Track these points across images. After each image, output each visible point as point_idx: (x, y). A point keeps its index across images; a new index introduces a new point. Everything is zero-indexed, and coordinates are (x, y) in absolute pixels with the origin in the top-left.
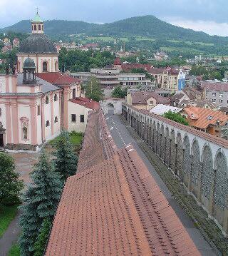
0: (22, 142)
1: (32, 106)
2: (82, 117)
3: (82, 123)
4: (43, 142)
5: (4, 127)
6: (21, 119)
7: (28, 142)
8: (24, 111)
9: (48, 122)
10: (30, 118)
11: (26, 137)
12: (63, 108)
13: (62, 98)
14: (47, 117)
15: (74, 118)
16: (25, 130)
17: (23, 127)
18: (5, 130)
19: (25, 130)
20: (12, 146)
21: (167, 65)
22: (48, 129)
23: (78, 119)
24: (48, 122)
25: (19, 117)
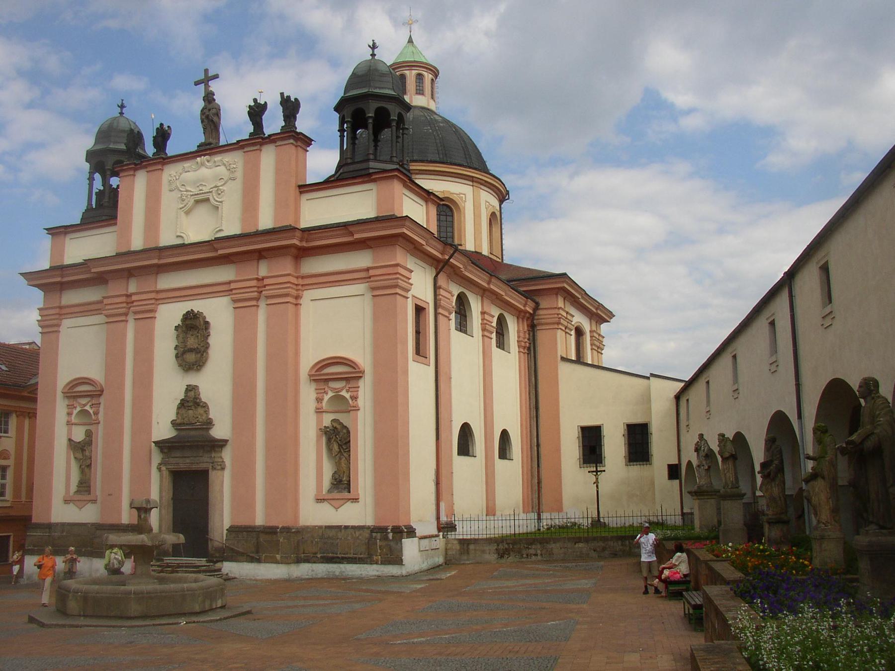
0: (314, 513)
2: (638, 440)
3: (636, 470)
4: (446, 528)
5: (220, 431)
6: (73, 391)
7: (357, 513)
8: (334, 320)
9: (466, 431)
11: (342, 483)
13: (530, 350)
16: (338, 440)
17: (327, 420)
18: (220, 444)
19: (338, 440)
20: (257, 542)
22: (466, 472)
23: (614, 446)
24: (466, 431)
25: (309, 358)
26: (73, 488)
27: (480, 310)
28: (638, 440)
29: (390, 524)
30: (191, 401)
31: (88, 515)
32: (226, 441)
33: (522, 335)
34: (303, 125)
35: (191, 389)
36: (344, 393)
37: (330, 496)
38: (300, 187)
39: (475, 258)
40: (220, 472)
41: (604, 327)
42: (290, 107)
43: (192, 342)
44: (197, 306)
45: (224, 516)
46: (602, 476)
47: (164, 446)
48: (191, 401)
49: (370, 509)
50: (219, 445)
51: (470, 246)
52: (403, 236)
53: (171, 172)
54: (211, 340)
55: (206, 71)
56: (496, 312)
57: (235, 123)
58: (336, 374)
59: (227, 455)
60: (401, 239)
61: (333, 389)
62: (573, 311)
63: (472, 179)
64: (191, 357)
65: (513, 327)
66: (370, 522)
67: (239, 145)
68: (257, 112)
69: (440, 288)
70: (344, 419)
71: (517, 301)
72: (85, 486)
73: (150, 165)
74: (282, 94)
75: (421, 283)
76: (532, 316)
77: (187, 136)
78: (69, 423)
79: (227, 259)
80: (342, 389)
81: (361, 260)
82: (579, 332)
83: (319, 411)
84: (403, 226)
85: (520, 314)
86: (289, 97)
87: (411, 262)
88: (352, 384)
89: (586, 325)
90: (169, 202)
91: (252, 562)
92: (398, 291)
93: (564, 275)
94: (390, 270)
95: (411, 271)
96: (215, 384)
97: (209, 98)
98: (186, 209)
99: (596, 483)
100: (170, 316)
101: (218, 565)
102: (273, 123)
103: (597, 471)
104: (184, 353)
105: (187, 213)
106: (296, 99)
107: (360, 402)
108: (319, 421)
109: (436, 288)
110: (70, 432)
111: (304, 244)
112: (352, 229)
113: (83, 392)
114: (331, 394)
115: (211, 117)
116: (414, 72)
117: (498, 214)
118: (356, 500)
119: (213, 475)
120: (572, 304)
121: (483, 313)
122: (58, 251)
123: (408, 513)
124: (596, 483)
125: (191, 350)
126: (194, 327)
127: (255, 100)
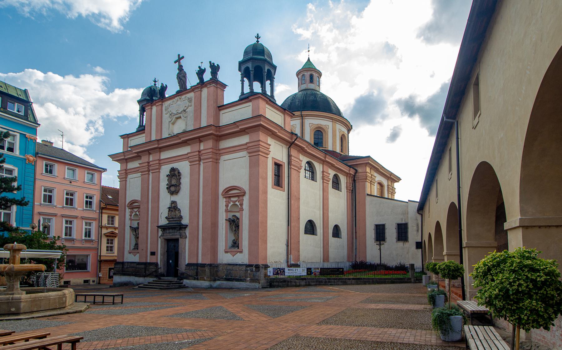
0: (225, 258)
2: (402, 232)
3: (401, 244)
5: (185, 221)
6: (229, 192)
7: (242, 258)
9: (336, 228)
10: (246, 188)
11: (236, 245)
16: (234, 224)
17: (230, 215)
18: (186, 226)
19: (234, 224)
23: (391, 233)
25: (222, 186)
26: (132, 247)
27: (321, 170)
28: (402, 232)
29: (254, 263)
30: (173, 207)
31: (136, 258)
32: (187, 226)
33: (348, 184)
34: (221, 77)
35: (173, 202)
36: (237, 203)
37: (230, 250)
38: (219, 107)
39: (333, 154)
40: (184, 240)
41: (396, 185)
42: (215, 69)
43: (174, 182)
44: (175, 165)
45: (186, 258)
46: (382, 246)
47: (164, 228)
48: (173, 207)
49: (247, 256)
50: (183, 227)
51: (330, 148)
52: (260, 125)
53: (166, 104)
54: (182, 181)
55: (179, 55)
56: (332, 173)
57: (192, 80)
58: (235, 193)
59: (187, 231)
60: (261, 128)
61: (233, 201)
62: (375, 174)
63: (332, 118)
64: (173, 189)
65: (343, 180)
66: (246, 262)
67: (193, 89)
68: (201, 73)
69: (291, 156)
70: (238, 215)
71: (345, 169)
72: (136, 246)
73: (157, 103)
74: (210, 62)
75: (277, 152)
76: (354, 176)
77: (172, 89)
78: (131, 219)
79: (185, 143)
80: (236, 201)
81: (244, 140)
82: (381, 185)
83: (227, 211)
84: (260, 120)
85: (347, 174)
86: (214, 64)
87: (270, 141)
88: (241, 198)
89: (385, 182)
90: (166, 118)
91: (365, 284)
92: (260, 153)
93: (369, 157)
94: (256, 143)
95: (270, 145)
96: (183, 200)
97: (181, 68)
98: (172, 121)
99: (380, 249)
100: (165, 170)
101: (182, 281)
102: (207, 76)
103: (380, 244)
104: (170, 187)
105: (173, 124)
106: (218, 65)
107: (244, 207)
108: (226, 216)
109: (289, 156)
110: (131, 223)
111: (218, 133)
112: (238, 124)
113: (133, 205)
114: (232, 203)
115: (182, 77)
116: (309, 73)
117: (346, 136)
118: (241, 252)
119: (181, 241)
120: (375, 171)
121: (323, 172)
122: (125, 144)
123: (266, 258)
124: (380, 249)
125: (173, 185)
126: (175, 174)
127: (200, 67)
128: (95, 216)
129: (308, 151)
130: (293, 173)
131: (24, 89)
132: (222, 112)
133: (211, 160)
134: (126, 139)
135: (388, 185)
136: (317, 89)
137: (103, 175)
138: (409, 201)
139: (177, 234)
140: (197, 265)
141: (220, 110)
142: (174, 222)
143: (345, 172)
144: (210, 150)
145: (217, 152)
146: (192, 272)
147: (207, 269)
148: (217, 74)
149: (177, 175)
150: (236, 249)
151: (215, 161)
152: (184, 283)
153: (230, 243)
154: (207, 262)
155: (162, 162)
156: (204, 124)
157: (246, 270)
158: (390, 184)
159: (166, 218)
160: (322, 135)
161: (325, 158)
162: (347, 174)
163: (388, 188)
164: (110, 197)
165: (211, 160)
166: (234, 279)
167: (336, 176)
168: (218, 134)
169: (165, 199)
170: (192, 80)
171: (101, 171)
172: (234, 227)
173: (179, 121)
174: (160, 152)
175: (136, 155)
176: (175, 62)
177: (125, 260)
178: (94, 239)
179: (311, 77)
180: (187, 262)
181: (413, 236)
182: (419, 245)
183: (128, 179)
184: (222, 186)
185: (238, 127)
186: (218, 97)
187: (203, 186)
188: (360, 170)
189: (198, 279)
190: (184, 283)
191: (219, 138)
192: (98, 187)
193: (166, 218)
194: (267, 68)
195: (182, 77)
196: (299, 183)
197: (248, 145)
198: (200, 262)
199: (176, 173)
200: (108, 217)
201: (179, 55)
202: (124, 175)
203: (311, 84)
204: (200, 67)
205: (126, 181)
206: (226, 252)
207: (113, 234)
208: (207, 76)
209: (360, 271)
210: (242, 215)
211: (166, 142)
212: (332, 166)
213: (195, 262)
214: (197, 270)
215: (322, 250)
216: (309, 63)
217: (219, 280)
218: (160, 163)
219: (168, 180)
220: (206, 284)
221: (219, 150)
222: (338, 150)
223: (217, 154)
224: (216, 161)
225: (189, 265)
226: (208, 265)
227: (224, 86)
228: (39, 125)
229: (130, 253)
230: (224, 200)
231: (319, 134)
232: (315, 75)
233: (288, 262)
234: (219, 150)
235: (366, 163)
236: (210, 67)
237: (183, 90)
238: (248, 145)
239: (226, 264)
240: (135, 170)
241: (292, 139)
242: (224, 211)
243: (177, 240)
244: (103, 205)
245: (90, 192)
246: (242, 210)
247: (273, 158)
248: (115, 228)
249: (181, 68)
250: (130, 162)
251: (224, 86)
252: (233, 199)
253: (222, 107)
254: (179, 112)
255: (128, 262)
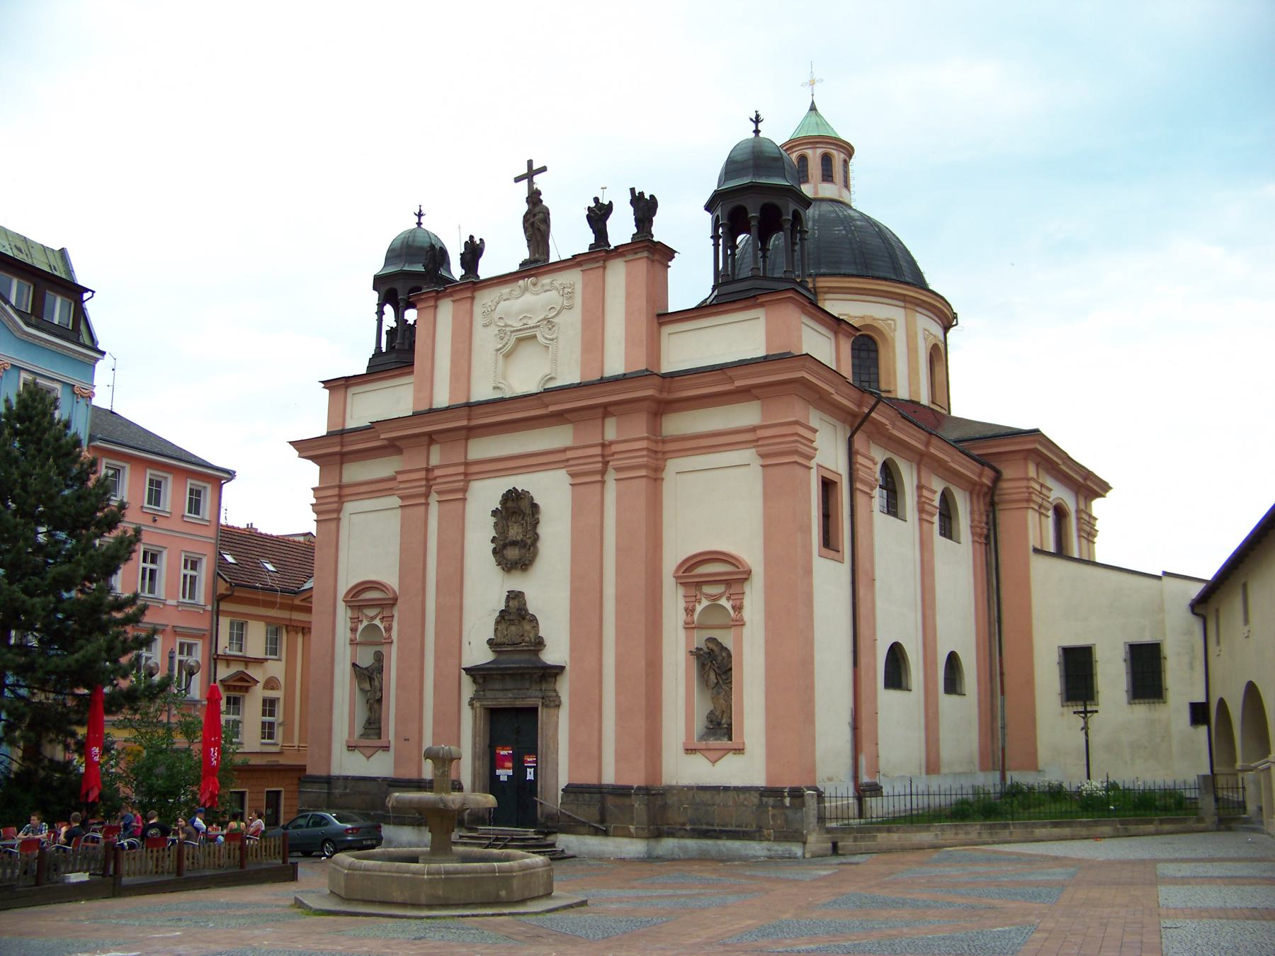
0: (686, 769)
1: (781, 453)
2: (1146, 668)
3: (1142, 711)
5: (554, 654)
6: (694, 573)
7: (745, 769)
9: (896, 655)
10: (753, 557)
11: (720, 727)
12: (674, 860)
13: (989, 539)
14: (894, 622)
15: (1078, 669)
16: (715, 666)
17: (699, 639)
18: (557, 671)
19: (715, 666)
21: (893, 822)
22: (897, 714)
23: (1112, 675)
24: (896, 655)
25: (674, 554)
26: (359, 730)
27: (915, 483)
28: (1146, 668)
29: (787, 782)
30: (515, 613)
36: (723, 602)
37: (703, 745)
38: (659, 316)
40: (552, 711)
41: (1097, 506)
42: (645, 208)
43: (515, 532)
44: (521, 482)
45: (562, 765)
46: (1094, 720)
48: (515, 613)
53: (485, 299)
55: (530, 163)
56: (938, 485)
57: (571, 236)
58: (712, 575)
59: (564, 687)
61: (708, 596)
62: (1050, 482)
63: (903, 298)
64: (513, 553)
66: (760, 780)
68: (599, 215)
69: (857, 453)
72: (374, 726)
74: (633, 190)
77: (506, 252)
78: (353, 642)
82: (1060, 513)
83: (689, 627)
85: (973, 488)
86: (642, 194)
87: (815, 418)
89: (1070, 503)
90: (485, 341)
93: (1037, 431)
95: (815, 431)
96: (548, 592)
97: (534, 198)
99: (1085, 728)
100: (486, 496)
101: (551, 839)
102: (621, 229)
104: (505, 546)
106: (652, 197)
107: (747, 614)
108: (689, 640)
109: (851, 453)
113: (365, 598)
114: (705, 603)
115: (537, 223)
116: (819, 152)
117: (942, 346)
118: (740, 751)
120: (1049, 473)
122: (337, 410)
124: (1085, 728)
126: (518, 513)
127: (596, 200)
128: (204, 624)
129: (895, 432)
130: (861, 499)
131: (57, 248)
132: (666, 330)
133: (643, 473)
134: (342, 392)
135: (1078, 511)
136: (846, 201)
137: (227, 488)
138: (1165, 573)
139: (533, 692)
140: (599, 791)
141: (661, 324)
142: (516, 657)
143: (969, 480)
144: (644, 444)
145: (660, 447)
146: (587, 813)
147: (638, 804)
148: (651, 222)
149: (528, 511)
150: (724, 743)
151: (651, 474)
152: (559, 847)
153: (700, 724)
154: (636, 779)
155: (473, 469)
156: (615, 365)
157: (761, 805)
158: (1082, 506)
159: (490, 642)
160: (876, 351)
161: (927, 445)
162: (974, 484)
163: (1078, 519)
164: (270, 567)
165: (643, 473)
166: (721, 832)
167: (946, 498)
168: (657, 397)
169: (486, 589)
170: (571, 236)
171: (220, 479)
172: (712, 676)
173: (527, 351)
174: (467, 439)
175: (385, 442)
176: (518, 180)
177: (336, 771)
178: (197, 697)
179: (827, 160)
180: (563, 781)
181: (1182, 683)
182: (1199, 713)
183: (345, 516)
184: (674, 554)
185: (731, 380)
186: (658, 288)
187: (619, 550)
188: (1008, 473)
189: (606, 833)
190: (559, 847)
191: (661, 408)
192: (211, 532)
193: (490, 642)
194: (792, 207)
195: (537, 223)
196: (871, 531)
197: (760, 433)
198: (609, 778)
199: (524, 504)
200: (232, 624)
201: (530, 163)
202: (329, 503)
203: (827, 186)
204: (596, 200)
205: (338, 519)
206: (689, 751)
207: (242, 680)
208: (621, 229)
209: (1008, 805)
210: (739, 640)
211: (487, 415)
212: (941, 469)
213: (592, 780)
214: (601, 807)
215: (923, 734)
216: (814, 119)
217: (671, 834)
218: (471, 472)
219: (496, 525)
220: (634, 847)
221: (664, 442)
222: (925, 400)
223: (659, 454)
224: (655, 476)
225: (569, 789)
226: (639, 788)
227: (669, 253)
228: (103, 353)
229: (351, 748)
230: (681, 591)
231: (866, 346)
232: (838, 157)
233: (856, 776)
234: (664, 442)
235: (1029, 451)
236: (632, 203)
237: (538, 264)
238: (760, 433)
239: (690, 788)
240: (373, 487)
241: (860, 405)
242: (681, 624)
243: (534, 710)
244: (222, 588)
245: (195, 549)
246: (740, 623)
247: (819, 466)
248: (248, 661)
249: (534, 198)
250: (351, 461)
251: (669, 253)
252: (707, 590)
253: (664, 318)
254: (531, 323)
255: (346, 778)
